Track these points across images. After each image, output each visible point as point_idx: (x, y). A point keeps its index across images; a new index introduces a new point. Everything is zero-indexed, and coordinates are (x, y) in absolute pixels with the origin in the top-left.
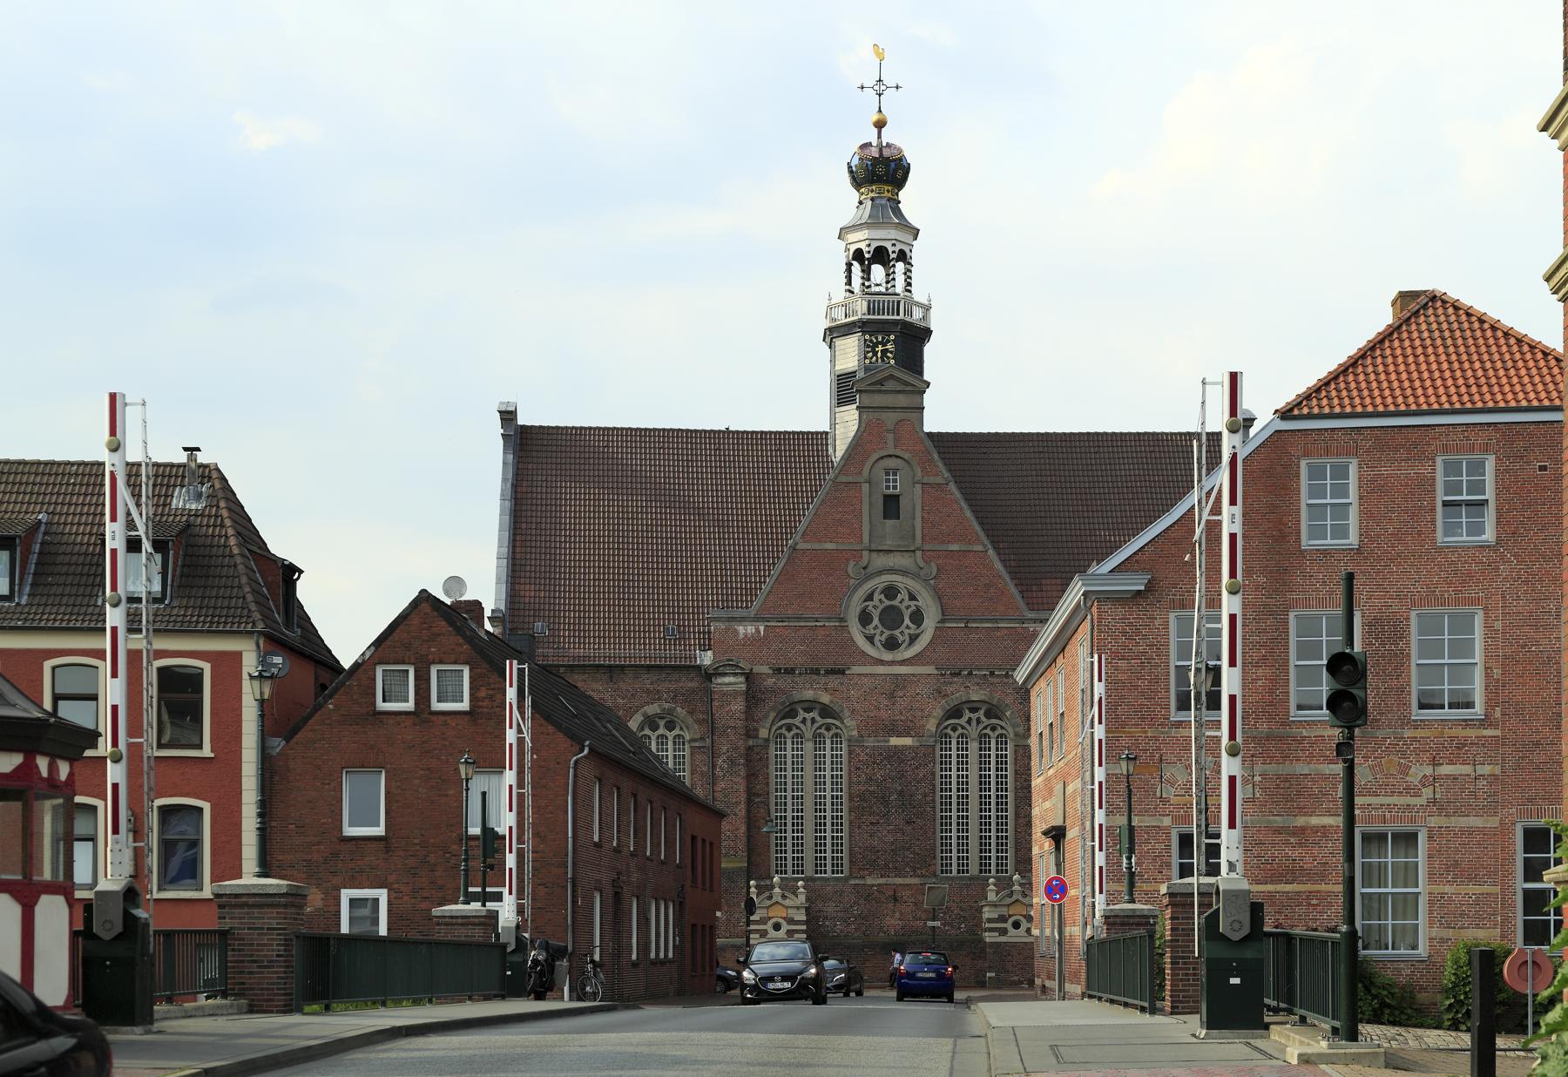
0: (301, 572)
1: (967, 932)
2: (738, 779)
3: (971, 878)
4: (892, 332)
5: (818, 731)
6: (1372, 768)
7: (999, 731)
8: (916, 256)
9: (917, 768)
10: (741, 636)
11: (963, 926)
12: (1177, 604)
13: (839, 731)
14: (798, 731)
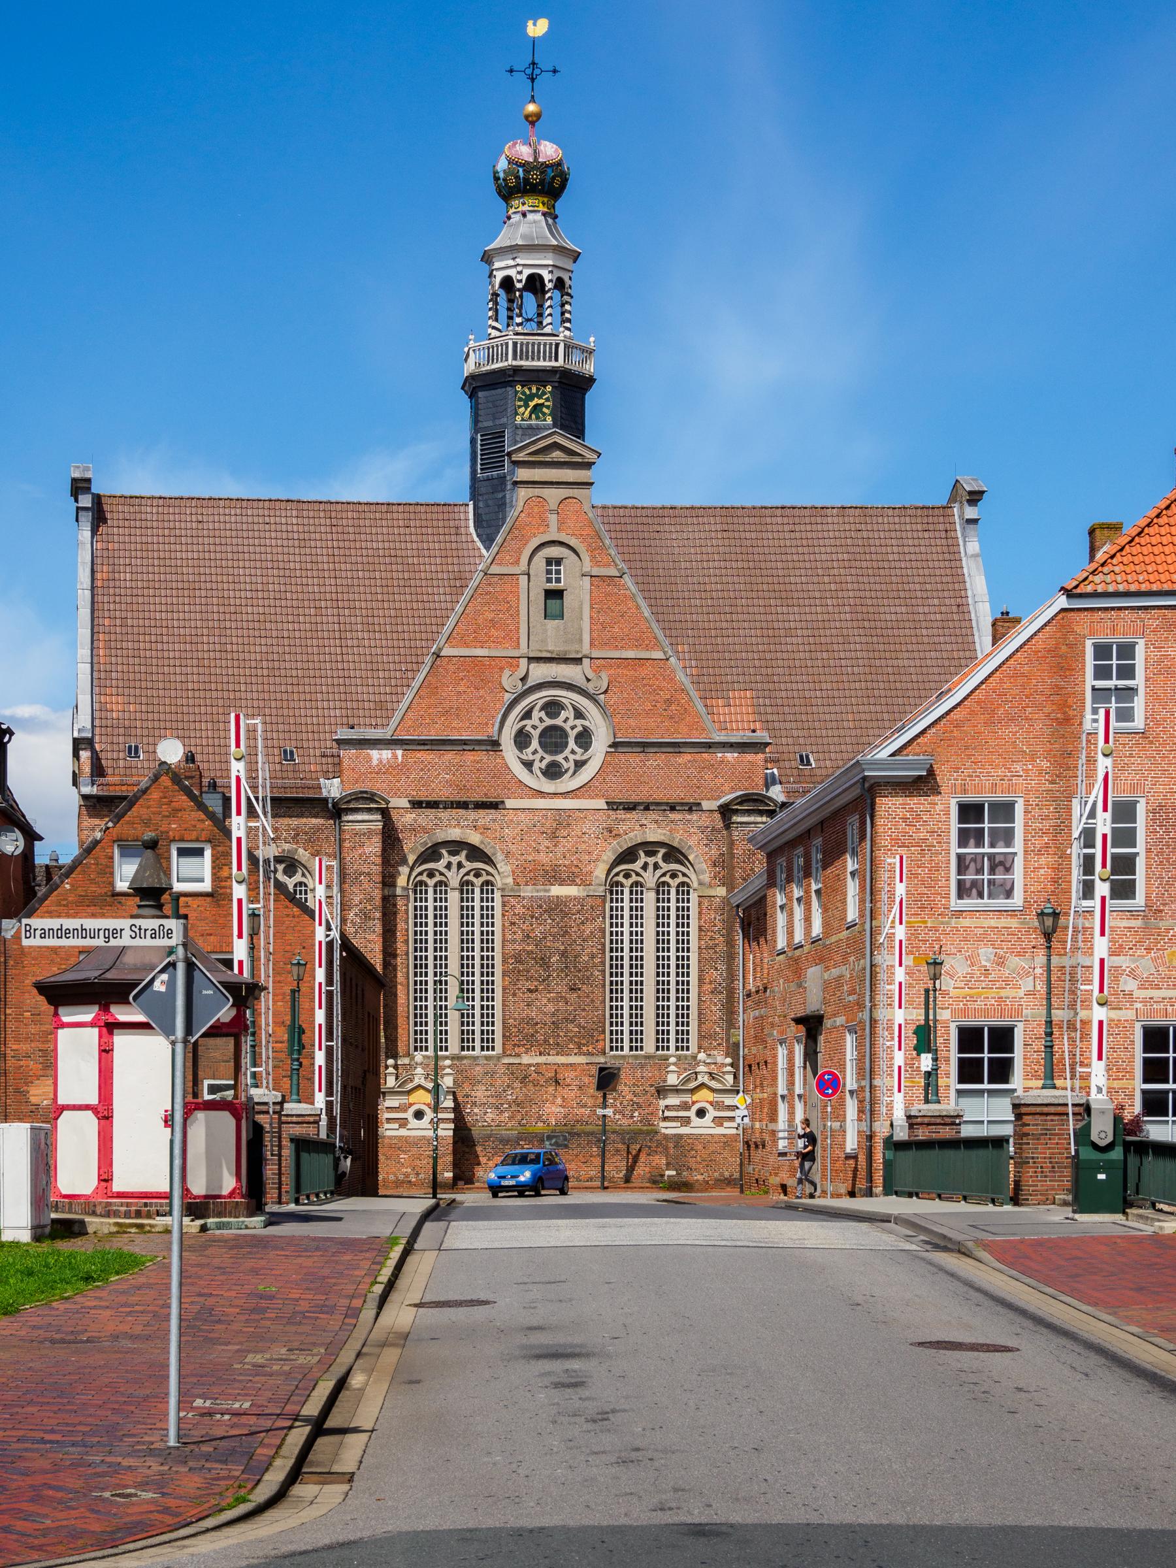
0: (12, 734)
1: (641, 1122)
2: (373, 937)
3: (648, 1057)
4: (549, 382)
5: (466, 878)
6: (1154, 960)
7: (681, 879)
8: (575, 285)
9: (583, 923)
10: (375, 762)
11: (636, 1114)
12: (959, 789)
13: (490, 878)
14: (443, 878)
